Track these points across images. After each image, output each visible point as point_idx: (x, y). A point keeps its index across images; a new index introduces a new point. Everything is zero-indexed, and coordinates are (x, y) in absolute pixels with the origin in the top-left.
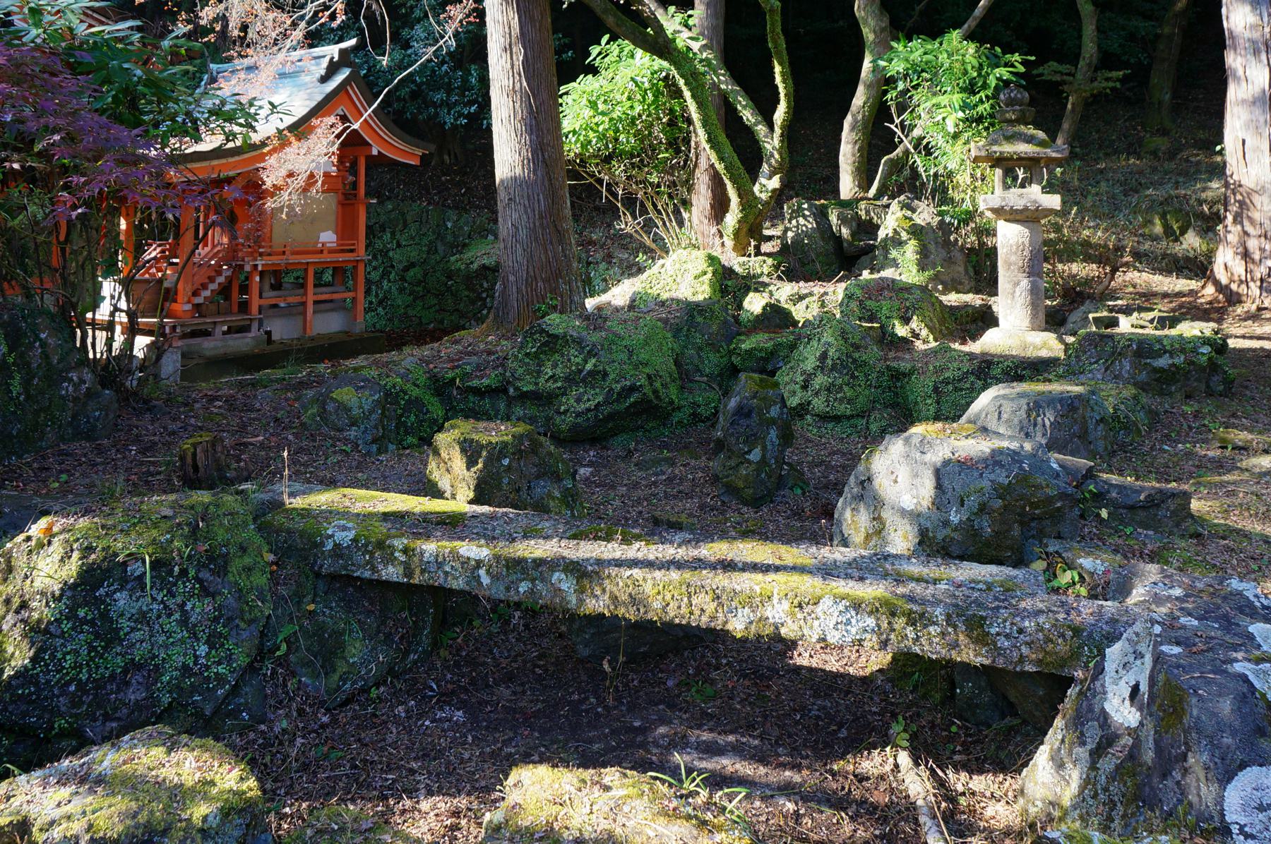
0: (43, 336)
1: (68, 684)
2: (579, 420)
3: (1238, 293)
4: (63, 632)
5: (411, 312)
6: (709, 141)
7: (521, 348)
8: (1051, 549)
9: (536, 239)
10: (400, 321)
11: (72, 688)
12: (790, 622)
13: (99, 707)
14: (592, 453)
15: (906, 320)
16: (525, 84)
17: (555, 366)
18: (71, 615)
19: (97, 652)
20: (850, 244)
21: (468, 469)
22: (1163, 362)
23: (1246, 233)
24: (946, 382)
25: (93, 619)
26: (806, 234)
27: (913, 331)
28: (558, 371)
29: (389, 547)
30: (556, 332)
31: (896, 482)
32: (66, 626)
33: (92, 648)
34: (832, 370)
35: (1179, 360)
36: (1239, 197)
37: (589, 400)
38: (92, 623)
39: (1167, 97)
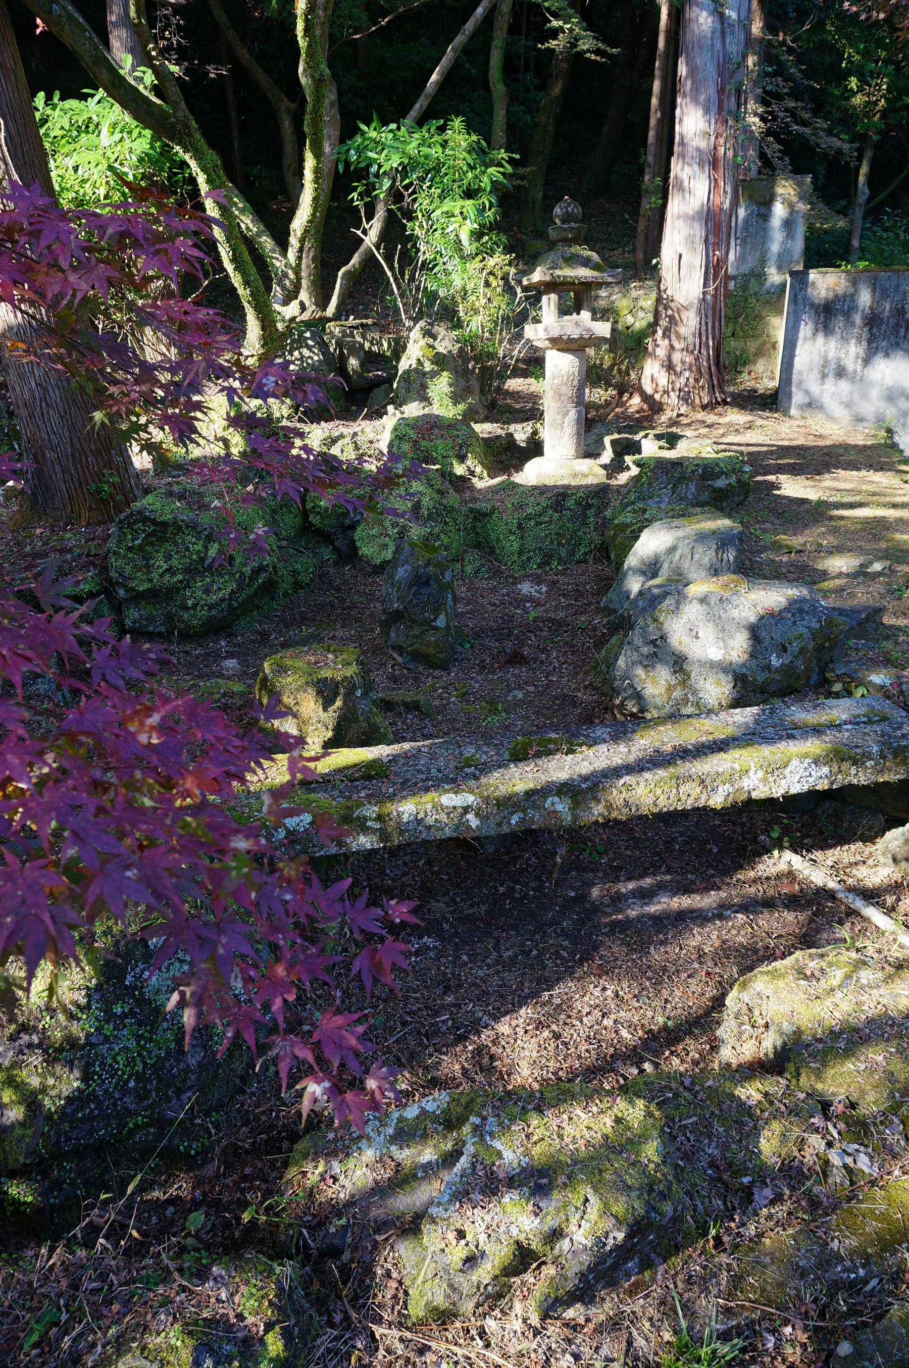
1: (127, 1082)
2: (213, 612)
3: (660, 403)
4: (106, 1037)
6: (233, 260)
7: (120, 542)
8: (839, 672)
11: (132, 1084)
12: (761, 786)
13: (168, 1086)
14: (223, 644)
15: (462, 459)
16: (16, 177)
17: (168, 558)
18: (109, 1016)
19: (145, 1038)
20: (360, 375)
21: (325, 709)
22: (721, 483)
23: (672, 347)
24: (528, 518)
25: (131, 1009)
26: (313, 367)
27: (469, 469)
28: (174, 562)
29: (358, 818)
30: (163, 518)
31: (697, 637)
32: (108, 1029)
33: (139, 1038)
34: (428, 519)
35: (733, 480)
36: (669, 312)
37: (220, 589)
38: (132, 1013)
39: (540, 195)
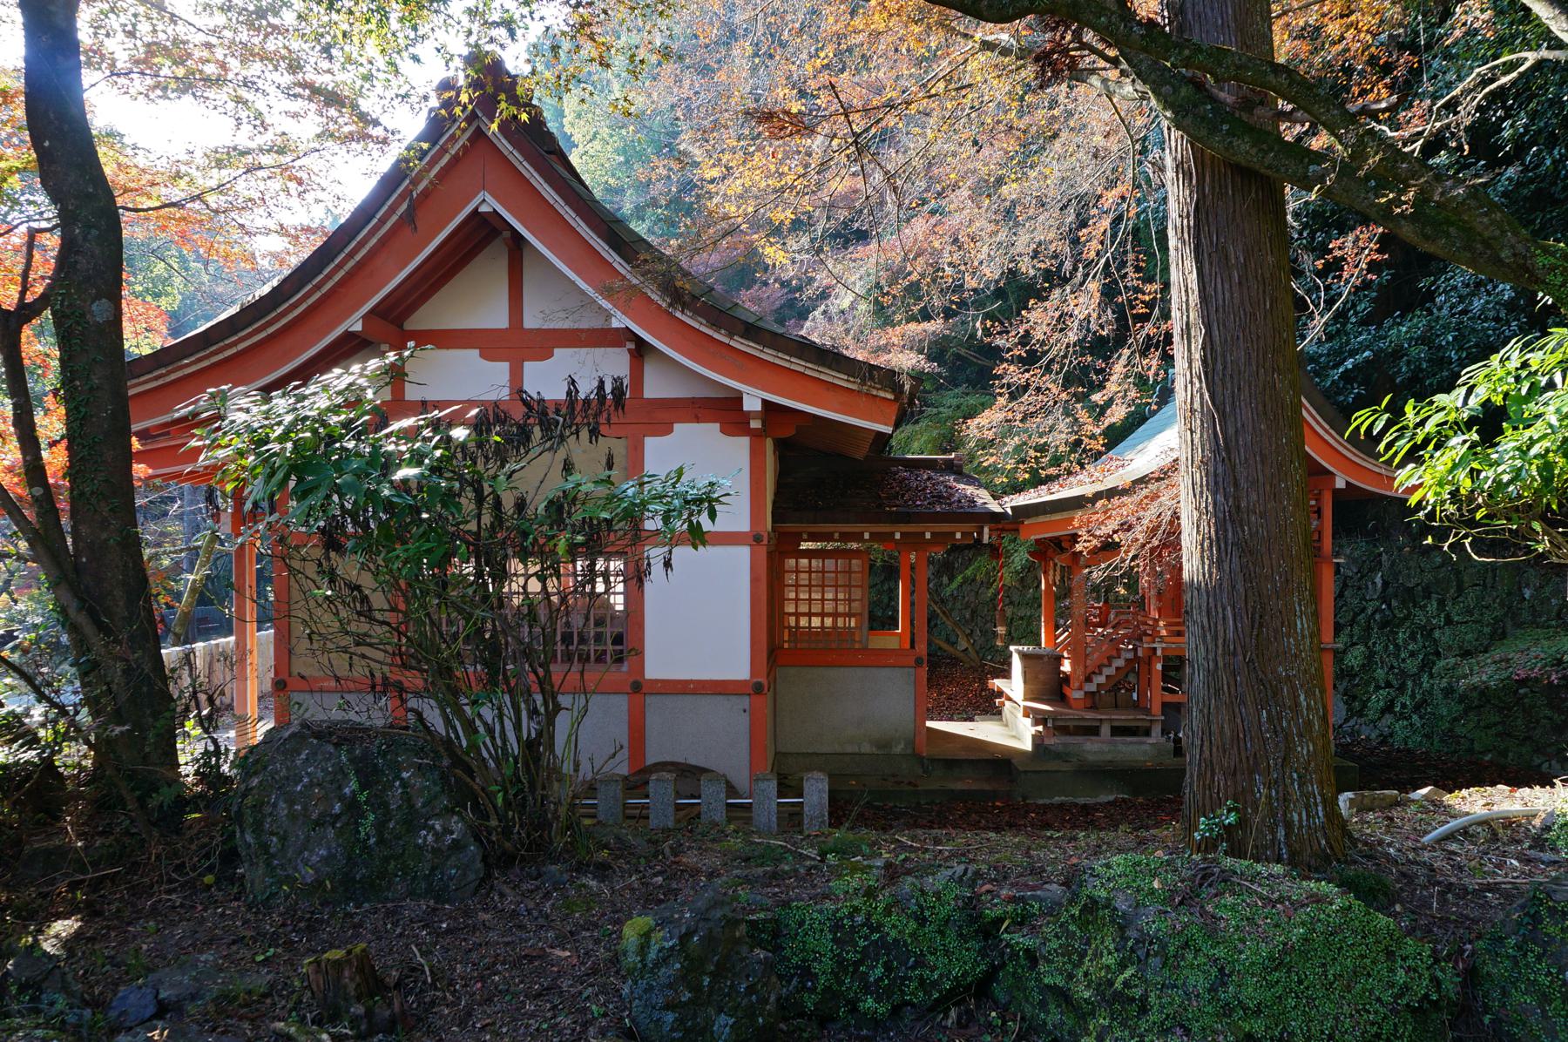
0: (405, 775)
5: (1459, 730)
9: (1217, 692)
10: (1442, 741)
16: (1207, 396)
